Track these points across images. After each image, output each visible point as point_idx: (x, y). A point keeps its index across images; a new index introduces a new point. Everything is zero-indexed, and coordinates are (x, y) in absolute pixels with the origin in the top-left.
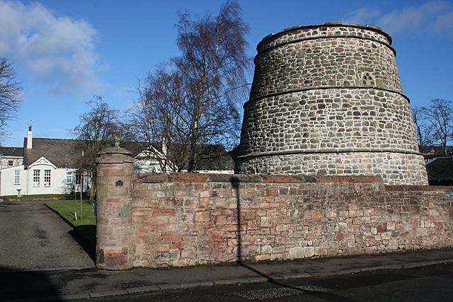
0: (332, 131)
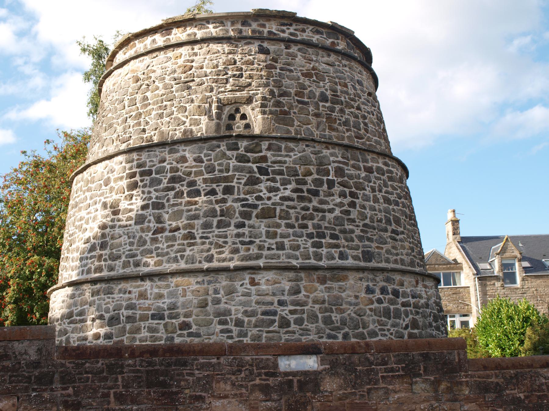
0: (143, 235)
